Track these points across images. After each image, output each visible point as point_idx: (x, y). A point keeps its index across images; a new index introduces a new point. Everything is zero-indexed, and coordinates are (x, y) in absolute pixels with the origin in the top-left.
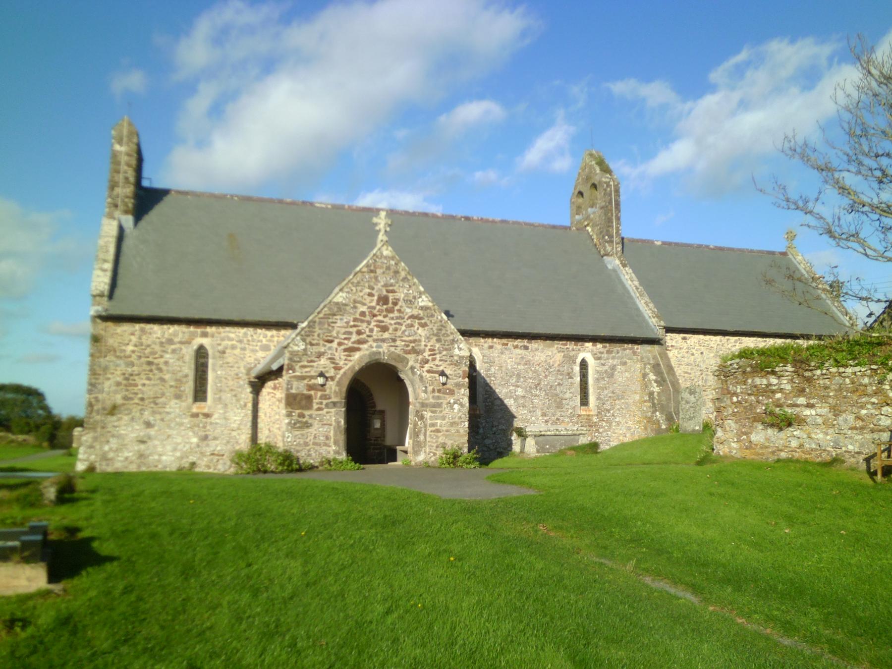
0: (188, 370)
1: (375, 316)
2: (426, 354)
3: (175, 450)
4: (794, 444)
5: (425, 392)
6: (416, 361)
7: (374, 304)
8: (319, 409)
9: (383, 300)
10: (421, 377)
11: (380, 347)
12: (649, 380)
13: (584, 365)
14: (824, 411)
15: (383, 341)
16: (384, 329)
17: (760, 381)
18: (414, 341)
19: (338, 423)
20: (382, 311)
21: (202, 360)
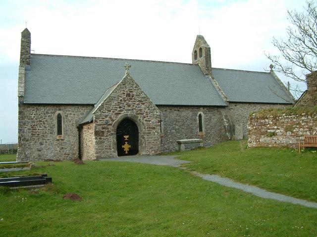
0: (55, 122)
1: (126, 101)
2: (145, 114)
3: (51, 153)
4: (273, 142)
5: (145, 128)
6: (141, 117)
7: (125, 97)
8: (107, 136)
9: (128, 95)
10: (143, 122)
11: (128, 112)
12: (224, 121)
13: (200, 116)
14: (282, 131)
15: (129, 110)
16: (129, 106)
17: (262, 121)
18: (140, 110)
19: (114, 141)
20: (128, 99)
21: (60, 119)
